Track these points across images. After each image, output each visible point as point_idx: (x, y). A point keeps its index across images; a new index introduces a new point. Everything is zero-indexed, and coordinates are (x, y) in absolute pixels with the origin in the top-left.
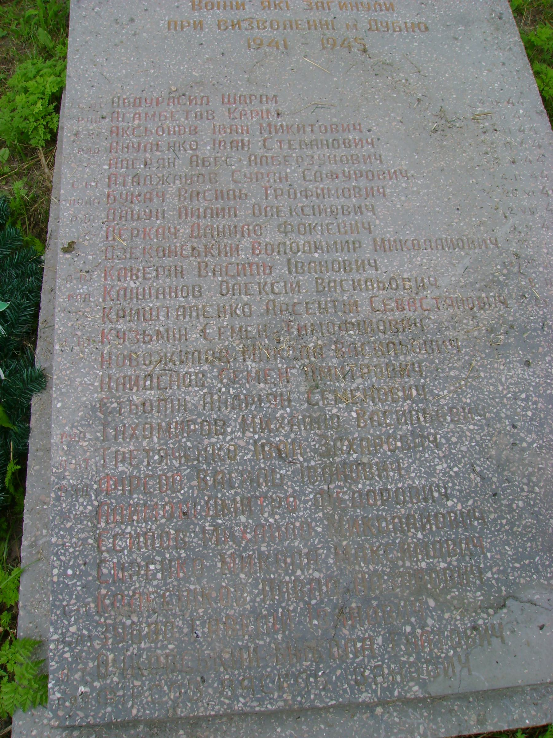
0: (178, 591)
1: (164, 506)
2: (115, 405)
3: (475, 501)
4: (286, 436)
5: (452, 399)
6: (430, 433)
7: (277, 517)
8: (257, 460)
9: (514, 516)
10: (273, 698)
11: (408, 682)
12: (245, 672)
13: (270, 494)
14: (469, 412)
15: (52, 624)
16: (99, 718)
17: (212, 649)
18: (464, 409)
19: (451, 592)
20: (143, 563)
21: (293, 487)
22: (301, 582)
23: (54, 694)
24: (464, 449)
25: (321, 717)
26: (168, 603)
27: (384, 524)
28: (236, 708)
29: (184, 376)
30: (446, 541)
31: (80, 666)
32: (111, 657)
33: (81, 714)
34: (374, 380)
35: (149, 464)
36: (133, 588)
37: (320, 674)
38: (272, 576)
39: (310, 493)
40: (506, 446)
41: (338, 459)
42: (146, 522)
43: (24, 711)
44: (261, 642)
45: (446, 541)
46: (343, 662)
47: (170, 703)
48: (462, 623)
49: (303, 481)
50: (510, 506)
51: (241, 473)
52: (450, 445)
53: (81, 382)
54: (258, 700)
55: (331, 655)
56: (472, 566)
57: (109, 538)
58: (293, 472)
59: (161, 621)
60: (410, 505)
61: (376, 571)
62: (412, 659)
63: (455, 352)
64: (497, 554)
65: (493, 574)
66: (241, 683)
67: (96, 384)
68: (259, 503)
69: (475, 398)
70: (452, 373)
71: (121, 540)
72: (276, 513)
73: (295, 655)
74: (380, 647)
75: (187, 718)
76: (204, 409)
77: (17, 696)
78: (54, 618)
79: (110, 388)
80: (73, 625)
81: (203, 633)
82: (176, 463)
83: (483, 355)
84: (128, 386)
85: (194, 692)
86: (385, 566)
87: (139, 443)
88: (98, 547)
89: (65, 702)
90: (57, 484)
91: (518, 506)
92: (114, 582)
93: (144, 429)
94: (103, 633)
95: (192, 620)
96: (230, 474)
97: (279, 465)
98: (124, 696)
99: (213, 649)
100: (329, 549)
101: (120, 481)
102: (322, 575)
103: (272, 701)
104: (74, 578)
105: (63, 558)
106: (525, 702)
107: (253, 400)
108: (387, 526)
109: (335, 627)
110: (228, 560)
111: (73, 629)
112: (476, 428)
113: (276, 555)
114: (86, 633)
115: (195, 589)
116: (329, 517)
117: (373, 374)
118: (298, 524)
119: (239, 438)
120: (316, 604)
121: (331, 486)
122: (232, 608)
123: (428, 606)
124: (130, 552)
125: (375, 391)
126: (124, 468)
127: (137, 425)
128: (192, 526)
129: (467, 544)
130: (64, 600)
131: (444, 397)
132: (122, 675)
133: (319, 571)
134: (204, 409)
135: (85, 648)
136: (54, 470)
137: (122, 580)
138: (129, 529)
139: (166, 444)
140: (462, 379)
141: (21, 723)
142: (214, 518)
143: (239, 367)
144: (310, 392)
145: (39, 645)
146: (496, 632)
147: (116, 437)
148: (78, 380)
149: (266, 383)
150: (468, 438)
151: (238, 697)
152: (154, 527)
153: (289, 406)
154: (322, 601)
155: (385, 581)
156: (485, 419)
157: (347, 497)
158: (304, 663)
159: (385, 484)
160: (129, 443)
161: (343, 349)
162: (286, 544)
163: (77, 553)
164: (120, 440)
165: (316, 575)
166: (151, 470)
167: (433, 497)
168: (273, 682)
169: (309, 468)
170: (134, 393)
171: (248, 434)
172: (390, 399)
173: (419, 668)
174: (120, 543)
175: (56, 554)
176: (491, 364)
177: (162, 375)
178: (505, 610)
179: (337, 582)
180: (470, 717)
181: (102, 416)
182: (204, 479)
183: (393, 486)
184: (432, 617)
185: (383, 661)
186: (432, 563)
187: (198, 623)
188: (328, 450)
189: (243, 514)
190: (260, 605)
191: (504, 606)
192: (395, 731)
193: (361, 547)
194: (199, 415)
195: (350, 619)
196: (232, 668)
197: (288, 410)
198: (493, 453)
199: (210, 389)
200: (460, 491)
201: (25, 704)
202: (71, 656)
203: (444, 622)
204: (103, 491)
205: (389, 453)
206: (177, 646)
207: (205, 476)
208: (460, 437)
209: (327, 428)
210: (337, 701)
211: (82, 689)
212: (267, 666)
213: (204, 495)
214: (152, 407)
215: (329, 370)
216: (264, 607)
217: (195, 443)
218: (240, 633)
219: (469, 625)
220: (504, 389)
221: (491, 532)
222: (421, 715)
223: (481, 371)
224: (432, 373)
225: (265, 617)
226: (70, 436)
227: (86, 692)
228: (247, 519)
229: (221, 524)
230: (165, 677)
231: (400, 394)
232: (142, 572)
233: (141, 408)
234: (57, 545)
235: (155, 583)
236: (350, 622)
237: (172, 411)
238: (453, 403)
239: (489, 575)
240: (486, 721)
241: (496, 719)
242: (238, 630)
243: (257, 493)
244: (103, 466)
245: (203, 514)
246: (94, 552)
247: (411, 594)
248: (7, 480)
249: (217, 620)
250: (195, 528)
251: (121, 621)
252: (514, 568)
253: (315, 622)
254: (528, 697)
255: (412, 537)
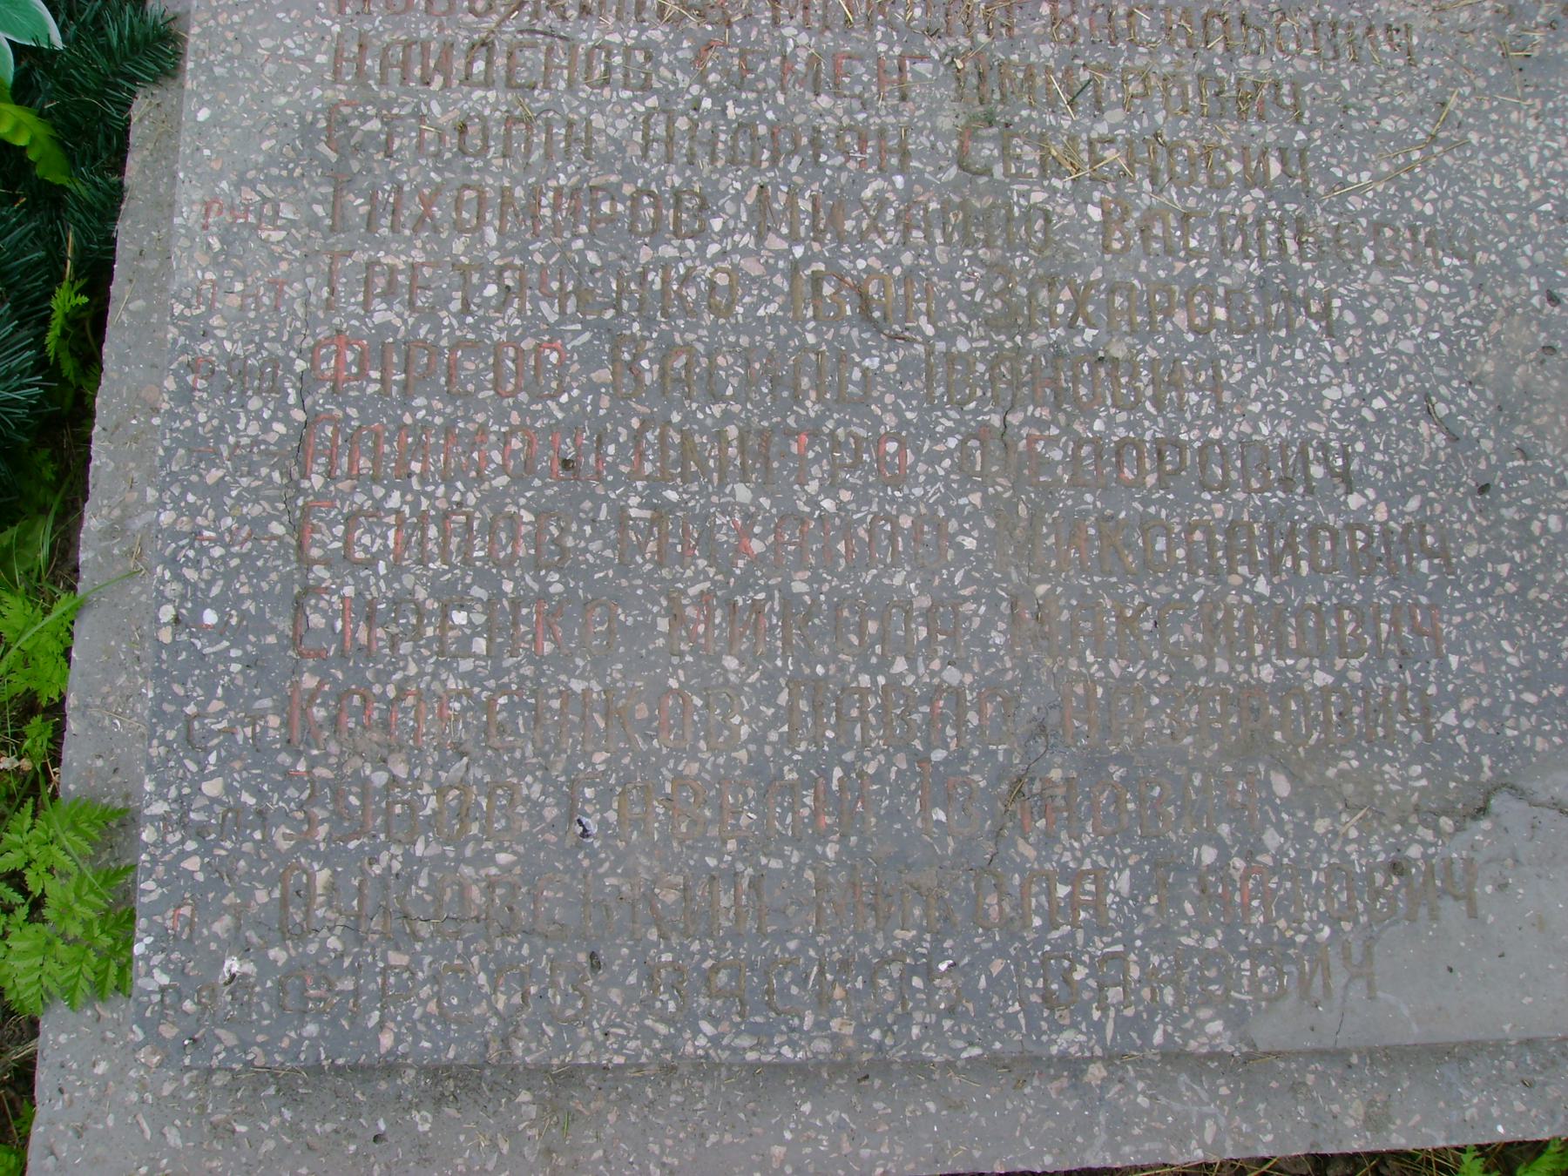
0: (534, 694)
1: (505, 439)
2: (375, 125)
3: (1426, 502)
4: (889, 258)
5: (1383, 198)
6: (1311, 292)
7: (845, 496)
8: (796, 320)
9: (1532, 557)
10: (799, 1029)
11: (1193, 1008)
12: (720, 948)
13: (830, 425)
14: (1428, 243)
15: (151, 768)
16: (283, 1052)
17: (625, 874)
18: (1414, 231)
19: (1338, 758)
20: (432, 605)
21: (897, 412)
22: (906, 693)
23: (149, 974)
24: (1406, 346)
25: (929, 1079)
26: (501, 729)
27: (1160, 545)
28: (689, 1049)
29: (589, 55)
30: (1337, 610)
31: (231, 899)
32: (323, 876)
33: (229, 1038)
34: (1160, 117)
35: (466, 309)
36: (398, 676)
37: (943, 967)
38: (820, 670)
39: (950, 432)
40: (1526, 351)
41: (1037, 341)
42: (449, 483)
43: (72, 1006)
44: (775, 864)
45: (1337, 610)
46: (1014, 937)
47: (494, 1022)
48: (1363, 850)
49: (929, 397)
50: (1523, 525)
51: (746, 357)
52: (1367, 330)
53: (273, 51)
54: (754, 1030)
55: (977, 916)
56: (1404, 688)
57: (332, 524)
58: (902, 366)
59: (478, 782)
60: (1239, 496)
61: (1127, 679)
62: (1211, 943)
63: (1400, 62)
64: (1475, 660)
65: (1460, 717)
66: (707, 977)
67: (321, 59)
68: (794, 449)
69: (1449, 204)
70: (1388, 125)
71: (370, 531)
72: (845, 485)
73: (874, 907)
74: (1124, 901)
75: (543, 1069)
76: (645, 157)
77: (51, 966)
78: (156, 751)
79: (360, 72)
80: (212, 775)
81: (603, 824)
82: (550, 312)
83: (1481, 83)
84: (417, 71)
85: (566, 995)
86: (1151, 665)
87: (441, 243)
88: (300, 546)
89: (181, 999)
90: (185, 350)
91: (1545, 529)
92: (342, 654)
93: (458, 204)
94: (300, 807)
95: (572, 783)
96: (711, 355)
97: (862, 341)
98: (356, 993)
99: (630, 874)
100: (994, 602)
101: (377, 352)
102: (968, 679)
103: (796, 1036)
104: (222, 635)
105: (191, 574)
106: (1501, 1077)
107: (795, 142)
108: (1170, 549)
109: (997, 835)
110: (691, 612)
111: (212, 788)
112: (1445, 290)
113: (836, 608)
114: (251, 801)
115: (587, 692)
116: (1001, 510)
117: (1157, 99)
118: (906, 522)
119: (745, 252)
120: (945, 762)
121: (1015, 419)
122: (693, 755)
123: (1272, 793)
124: (396, 569)
125: (1162, 151)
126: (390, 316)
127: (438, 190)
128: (587, 505)
129: (1394, 623)
130: (188, 698)
131: (1360, 191)
132: (355, 932)
133: (964, 667)
134: (645, 157)
135: (247, 847)
136: (178, 308)
137: (367, 652)
138: (395, 500)
139: (524, 252)
140: (1415, 143)
141: (63, 1038)
142: (657, 483)
143: (759, 42)
144: (968, 134)
145: (116, 824)
146: (1455, 883)
147: (371, 222)
148: (266, 43)
149: (837, 95)
150: (1421, 318)
151: (697, 1018)
152: (471, 499)
153: (902, 169)
154: (963, 756)
155: (1153, 712)
156: (1472, 266)
157: (1057, 455)
158: (898, 933)
159: (1171, 427)
160: (409, 240)
161: (1075, 20)
162: (868, 577)
163: (234, 562)
164: (385, 231)
165: (952, 675)
166: (474, 328)
167: (1308, 477)
168: (802, 981)
169: (950, 359)
170: (433, 95)
171: (775, 243)
172: (1202, 178)
173: (1230, 969)
174: (366, 540)
175: (172, 562)
176: (1502, 109)
177: (522, 46)
178: (1485, 824)
179: (1012, 701)
180: (1345, 1107)
181: (334, 157)
182: (632, 367)
183: (1195, 433)
184: (1279, 826)
185: (1128, 944)
186: (1292, 668)
187: (589, 793)
188: (1011, 311)
189: (745, 480)
190: (778, 753)
191: (1483, 811)
192: (1136, 1131)
193: (1089, 606)
194: (629, 173)
195: (1043, 814)
196: (685, 933)
197: (899, 180)
198: (1489, 367)
199: (667, 98)
200: (1388, 469)
201: (74, 988)
202: (203, 867)
203: (1313, 843)
204: (320, 381)
205: (1190, 338)
206: (521, 859)
207: (636, 358)
208: (1396, 313)
209: (1010, 246)
210: (987, 1047)
211: (233, 965)
212: (790, 935)
213: (628, 413)
214: (485, 139)
215: (1030, 76)
216: (789, 760)
217: (612, 256)
218: (713, 831)
219: (1381, 858)
220: (1531, 187)
221: (1466, 596)
222: (1214, 1094)
223: (1472, 128)
224: (1328, 115)
225: (792, 788)
226: (232, 208)
227: (245, 976)
228: (757, 493)
229: (676, 505)
230: (482, 945)
231: (1235, 167)
232: (430, 632)
233: (451, 140)
234: (176, 535)
235: (466, 665)
236: (1041, 823)
237: (548, 156)
238: (1384, 212)
239: (1450, 718)
240: (1390, 1120)
241: (1417, 1118)
242: (707, 823)
243: (791, 421)
244: (329, 305)
245: (624, 469)
246: (287, 562)
247: (1224, 754)
248: (52, 338)
249: (645, 789)
250: (597, 509)
251: (356, 772)
252: (1520, 706)
253: (939, 815)
254: (1510, 1064)
255: (1241, 590)
